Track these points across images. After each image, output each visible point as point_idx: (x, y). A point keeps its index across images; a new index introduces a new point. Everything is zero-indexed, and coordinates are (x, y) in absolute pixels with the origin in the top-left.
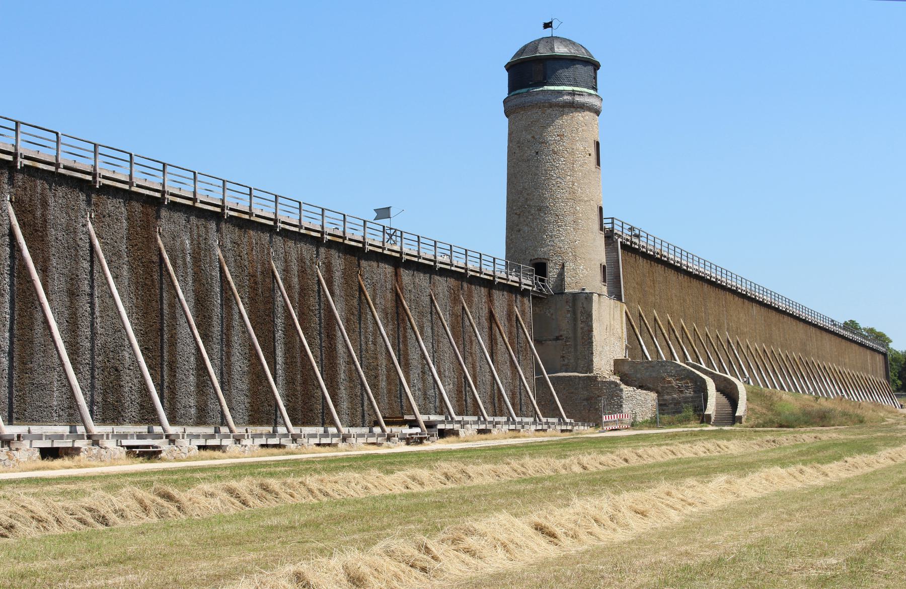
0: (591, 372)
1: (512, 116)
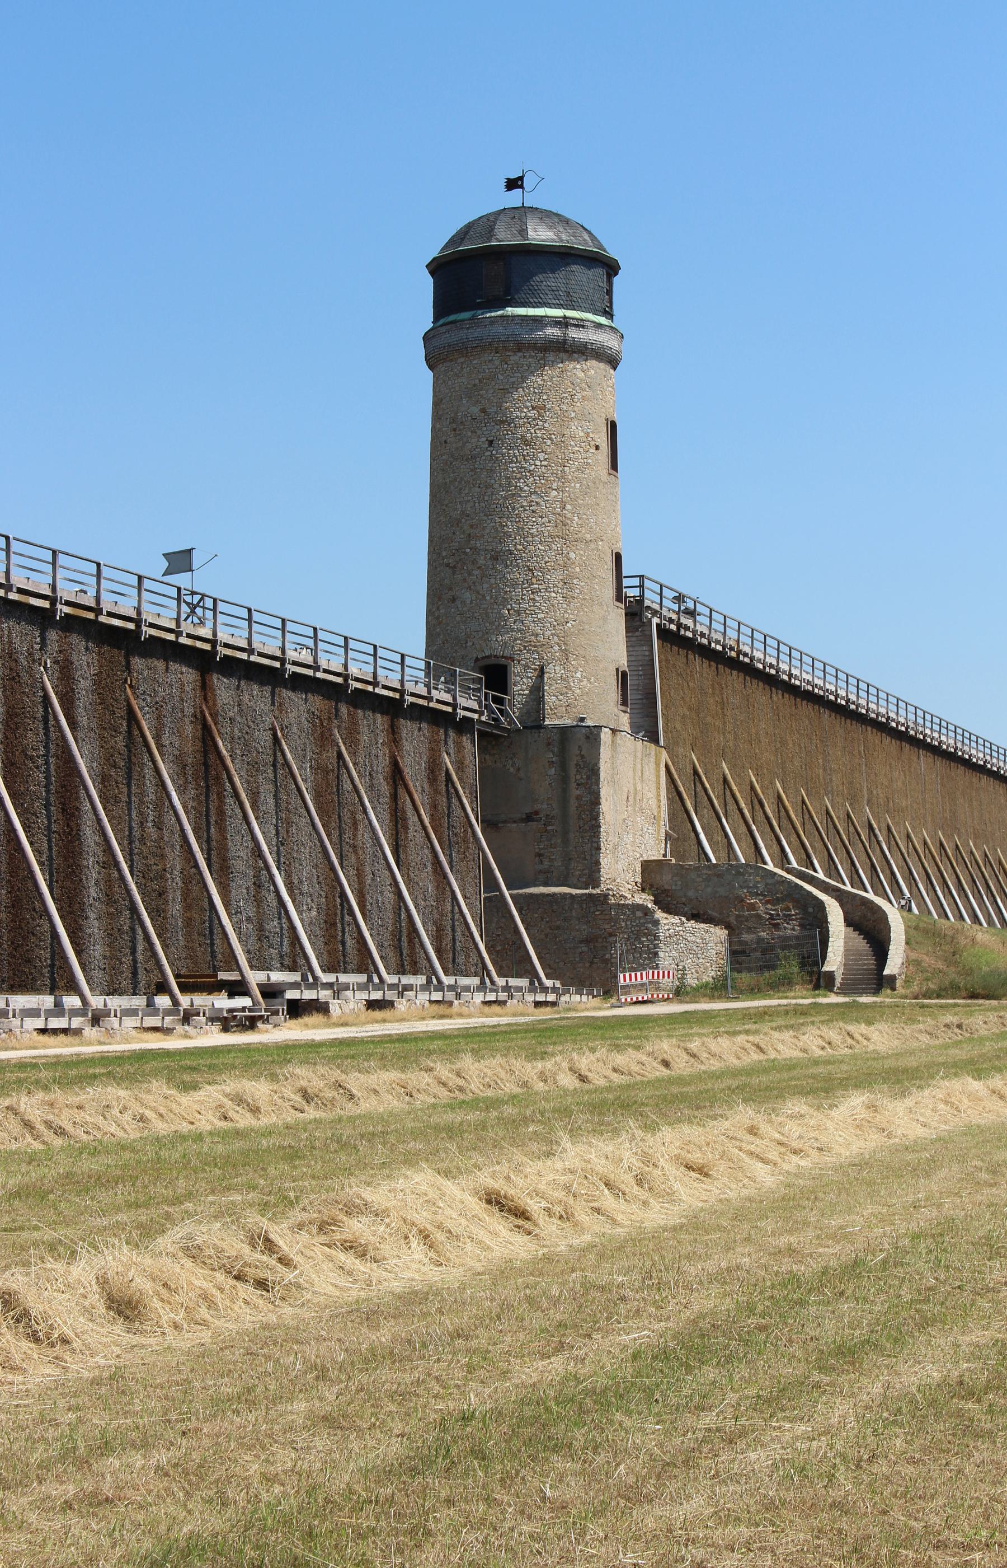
1: (442, 368)
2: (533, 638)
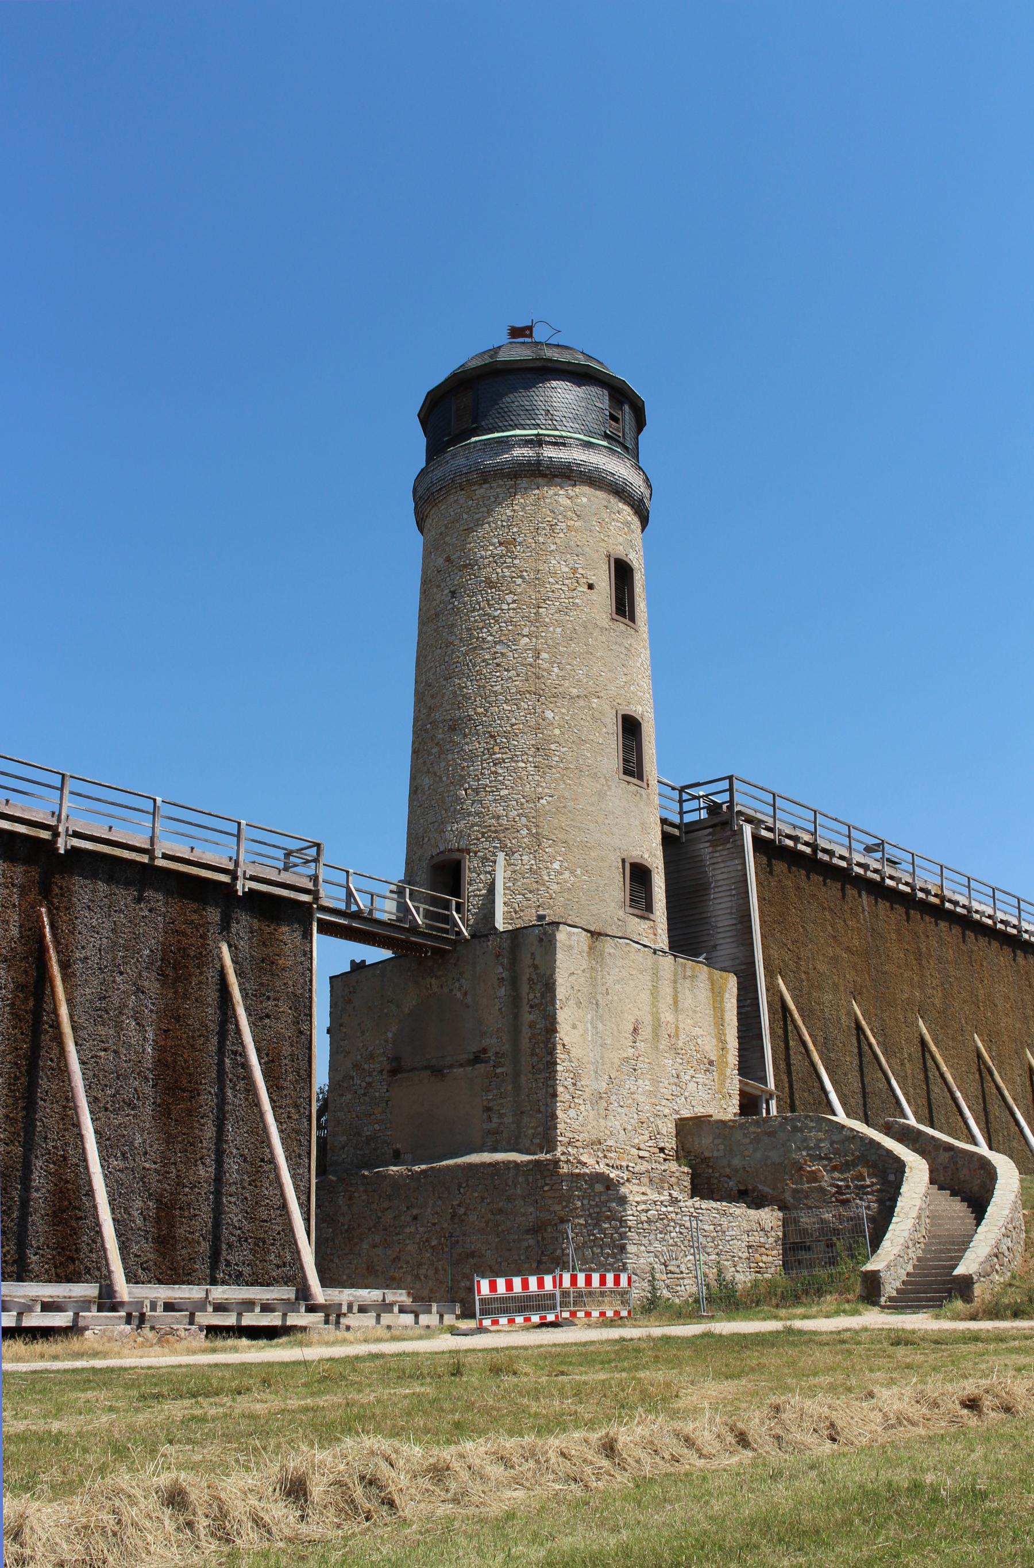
0: (552, 1149)
2: (493, 821)
